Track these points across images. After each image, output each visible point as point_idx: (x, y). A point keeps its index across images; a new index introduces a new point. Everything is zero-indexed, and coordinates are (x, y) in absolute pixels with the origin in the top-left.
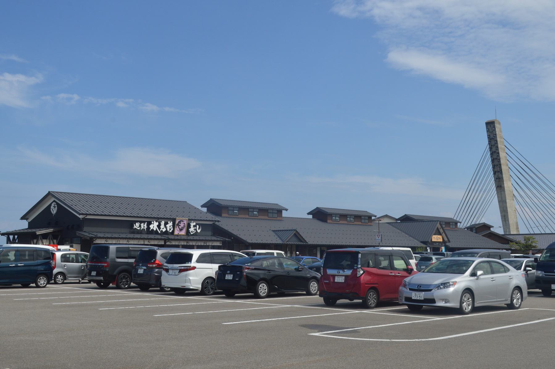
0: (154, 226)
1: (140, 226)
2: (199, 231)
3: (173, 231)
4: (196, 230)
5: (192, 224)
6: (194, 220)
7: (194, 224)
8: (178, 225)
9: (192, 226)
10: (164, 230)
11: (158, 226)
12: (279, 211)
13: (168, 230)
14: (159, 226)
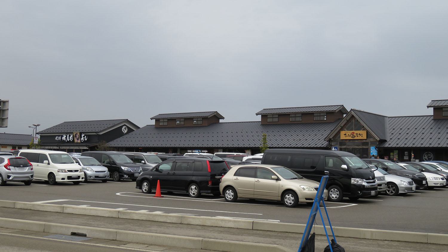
0: (64, 138)
1: (58, 138)
2: (86, 140)
3: (73, 140)
4: (84, 139)
5: (83, 135)
6: (84, 133)
7: (84, 135)
8: (76, 136)
9: (82, 137)
10: (68, 140)
11: (66, 137)
12: (213, 119)
13: (71, 140)
14: (66, 138)
